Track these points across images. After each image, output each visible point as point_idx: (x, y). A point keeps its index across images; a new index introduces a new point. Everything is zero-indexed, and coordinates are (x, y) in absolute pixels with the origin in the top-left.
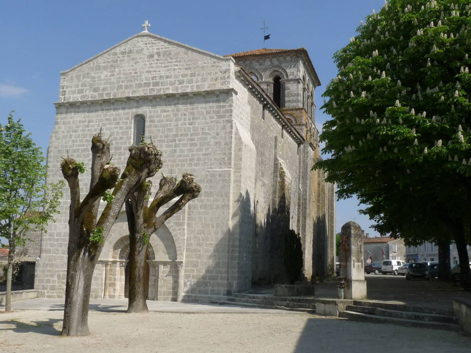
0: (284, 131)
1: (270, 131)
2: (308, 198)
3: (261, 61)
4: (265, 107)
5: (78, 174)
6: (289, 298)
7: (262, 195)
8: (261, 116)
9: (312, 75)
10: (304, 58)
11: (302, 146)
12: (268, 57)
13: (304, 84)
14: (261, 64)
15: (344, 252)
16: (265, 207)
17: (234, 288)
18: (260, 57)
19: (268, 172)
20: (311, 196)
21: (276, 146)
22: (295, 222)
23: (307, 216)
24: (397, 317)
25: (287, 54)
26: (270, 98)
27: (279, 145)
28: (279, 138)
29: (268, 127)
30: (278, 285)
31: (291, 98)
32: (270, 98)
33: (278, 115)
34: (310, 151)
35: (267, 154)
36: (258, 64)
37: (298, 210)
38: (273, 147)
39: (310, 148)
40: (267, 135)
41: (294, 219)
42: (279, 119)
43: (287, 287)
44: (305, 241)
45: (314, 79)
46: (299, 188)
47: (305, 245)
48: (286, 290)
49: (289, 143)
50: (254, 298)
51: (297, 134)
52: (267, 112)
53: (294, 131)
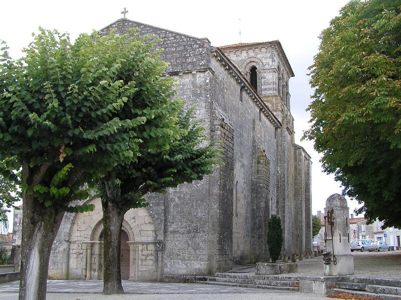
0: (262, 114)
1: (248, 114)
2: (286, 180)
3: (238, 53)
4: (242, 88)
5: (53, 145)
6: (271, 276)
7: (242, 175)
8: (238, 98)
9: (286, 66)
10: (278, 49)
11: (279, 130)
12: (244, 49)
13: (279, 74)
14: (238, 56)
15: (330, 226)
16: (245, 188)
17: (215, 265)
18: (236, 50)
19: (247, 153)
20: (289, 178)
21: (254, 128)
22: (274, 203)
23: (286, 197)
24: (391, 294)
25: (263, 46)
26: (247, 81)
27: (257, 127)
28: (257, 122)
29: (246, 109)
30: (259, 263)
31: (267, 87)
32: (247, 81)
33: (255, 97)
34: (287, 135)
35: (245, 135)
36: (235, 55)
37: (277, 192)
38: (251, 130)
39: (286, 133)
40: (245, 117)
41: (273, 200)
42: (256, 102)
43: (269, 265)
44: (284, 222)
45: (288, 70)
46: (278, 171)
47: (284, 225)
48: (268, 268)
49: (266, 127)
50: (235, 277)
51: (274, 118)
52: (244, 93)
53: (271, 115)
